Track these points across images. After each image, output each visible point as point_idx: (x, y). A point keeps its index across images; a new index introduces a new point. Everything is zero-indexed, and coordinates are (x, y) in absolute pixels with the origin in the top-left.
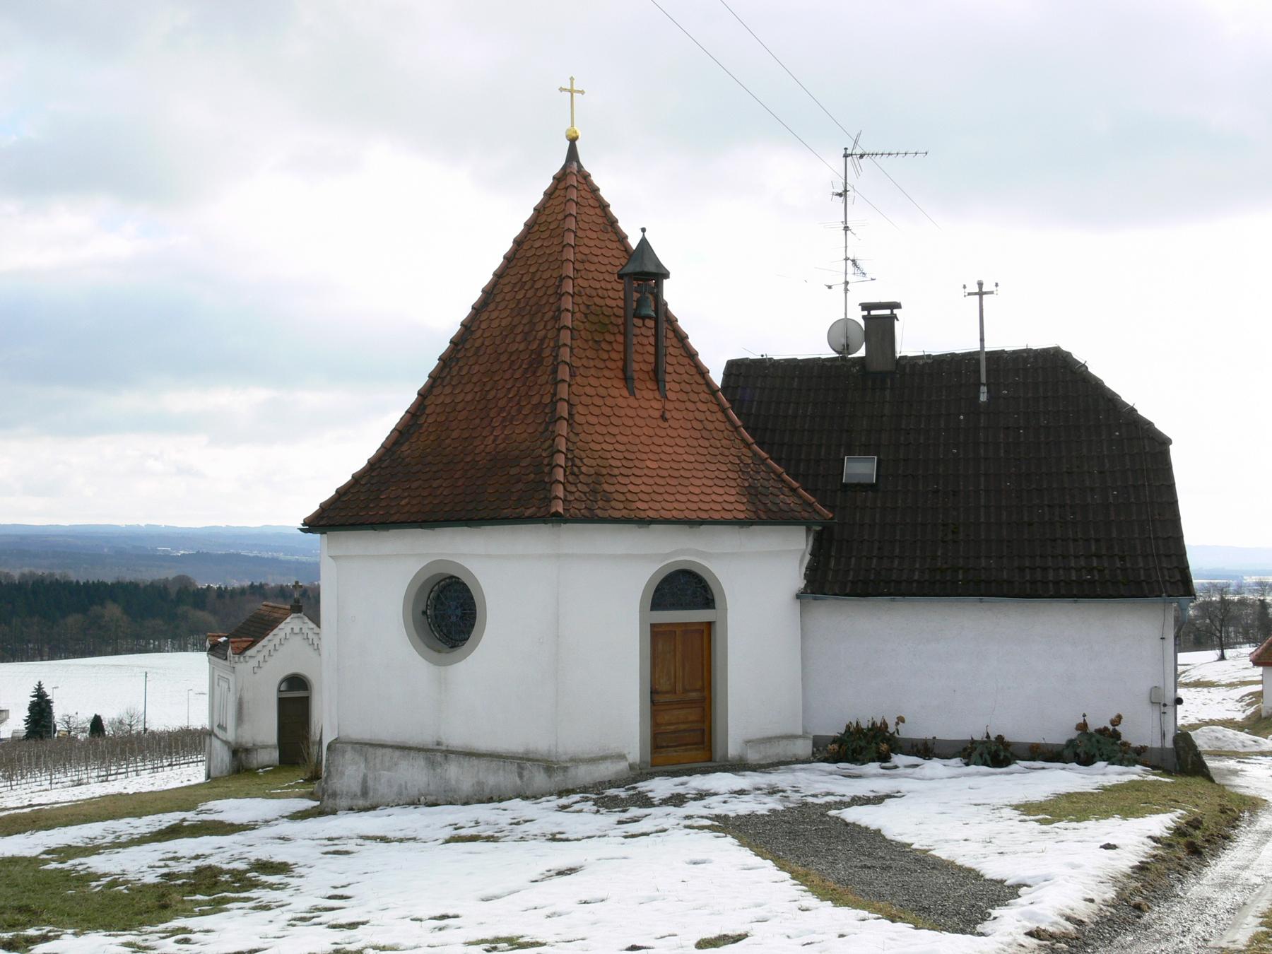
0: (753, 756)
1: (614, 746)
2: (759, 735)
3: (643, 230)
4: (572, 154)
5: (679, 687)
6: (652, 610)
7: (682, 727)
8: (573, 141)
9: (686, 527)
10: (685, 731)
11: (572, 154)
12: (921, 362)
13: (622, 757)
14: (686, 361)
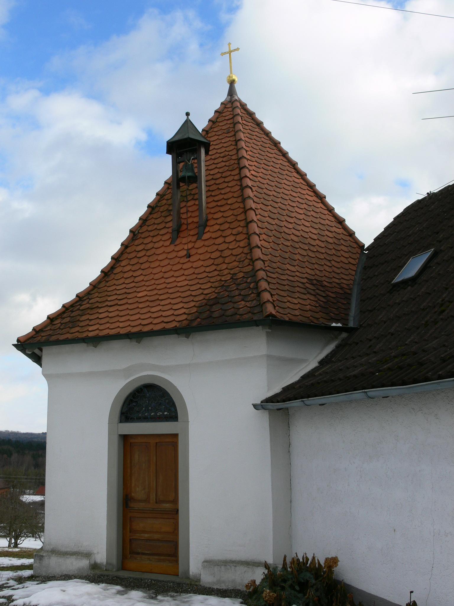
0: (207, 579)
1: (85, 545)
2: (238, 559)
3: (188, 114)
4: (232, 92)
5: (153, 497)
6: (121, 422)
7: (156, 536)
8: (232, 83)
9: (83, 346)
10: (158, 540)
11: (232, 92)
12: (450, 188)
13: (88, 555)
14: (348, 238)
